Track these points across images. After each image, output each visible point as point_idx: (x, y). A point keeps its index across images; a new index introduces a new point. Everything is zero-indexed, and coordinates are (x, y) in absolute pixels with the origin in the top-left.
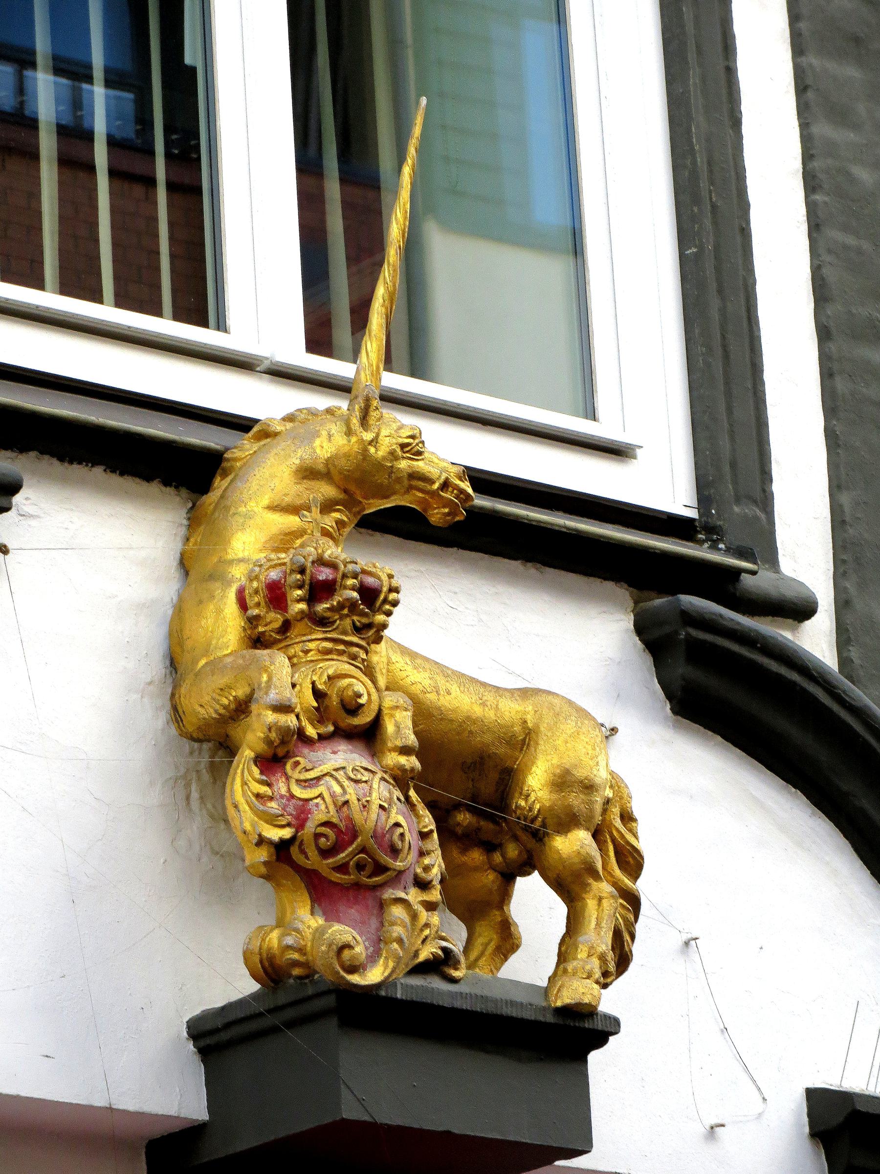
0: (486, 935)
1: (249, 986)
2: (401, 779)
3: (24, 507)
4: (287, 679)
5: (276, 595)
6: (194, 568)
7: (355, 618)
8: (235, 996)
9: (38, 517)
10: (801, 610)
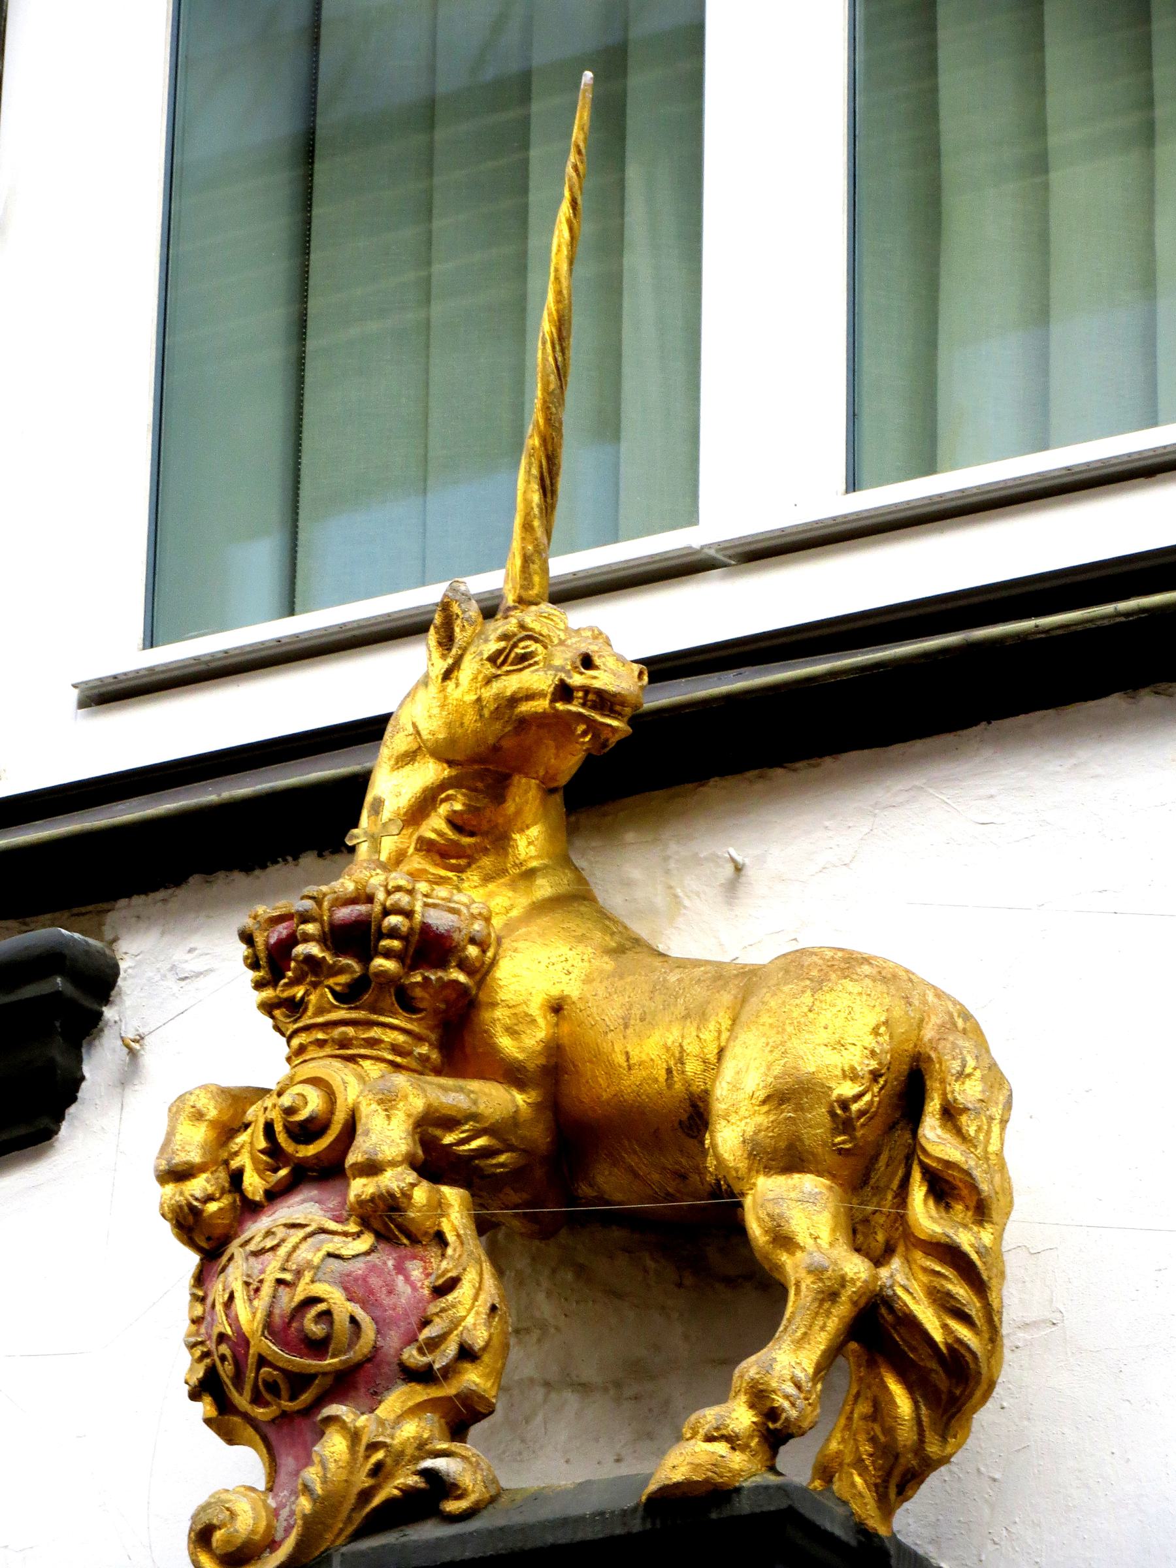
3: (184, 966)
7: (331, 982)
9: (211, 970)
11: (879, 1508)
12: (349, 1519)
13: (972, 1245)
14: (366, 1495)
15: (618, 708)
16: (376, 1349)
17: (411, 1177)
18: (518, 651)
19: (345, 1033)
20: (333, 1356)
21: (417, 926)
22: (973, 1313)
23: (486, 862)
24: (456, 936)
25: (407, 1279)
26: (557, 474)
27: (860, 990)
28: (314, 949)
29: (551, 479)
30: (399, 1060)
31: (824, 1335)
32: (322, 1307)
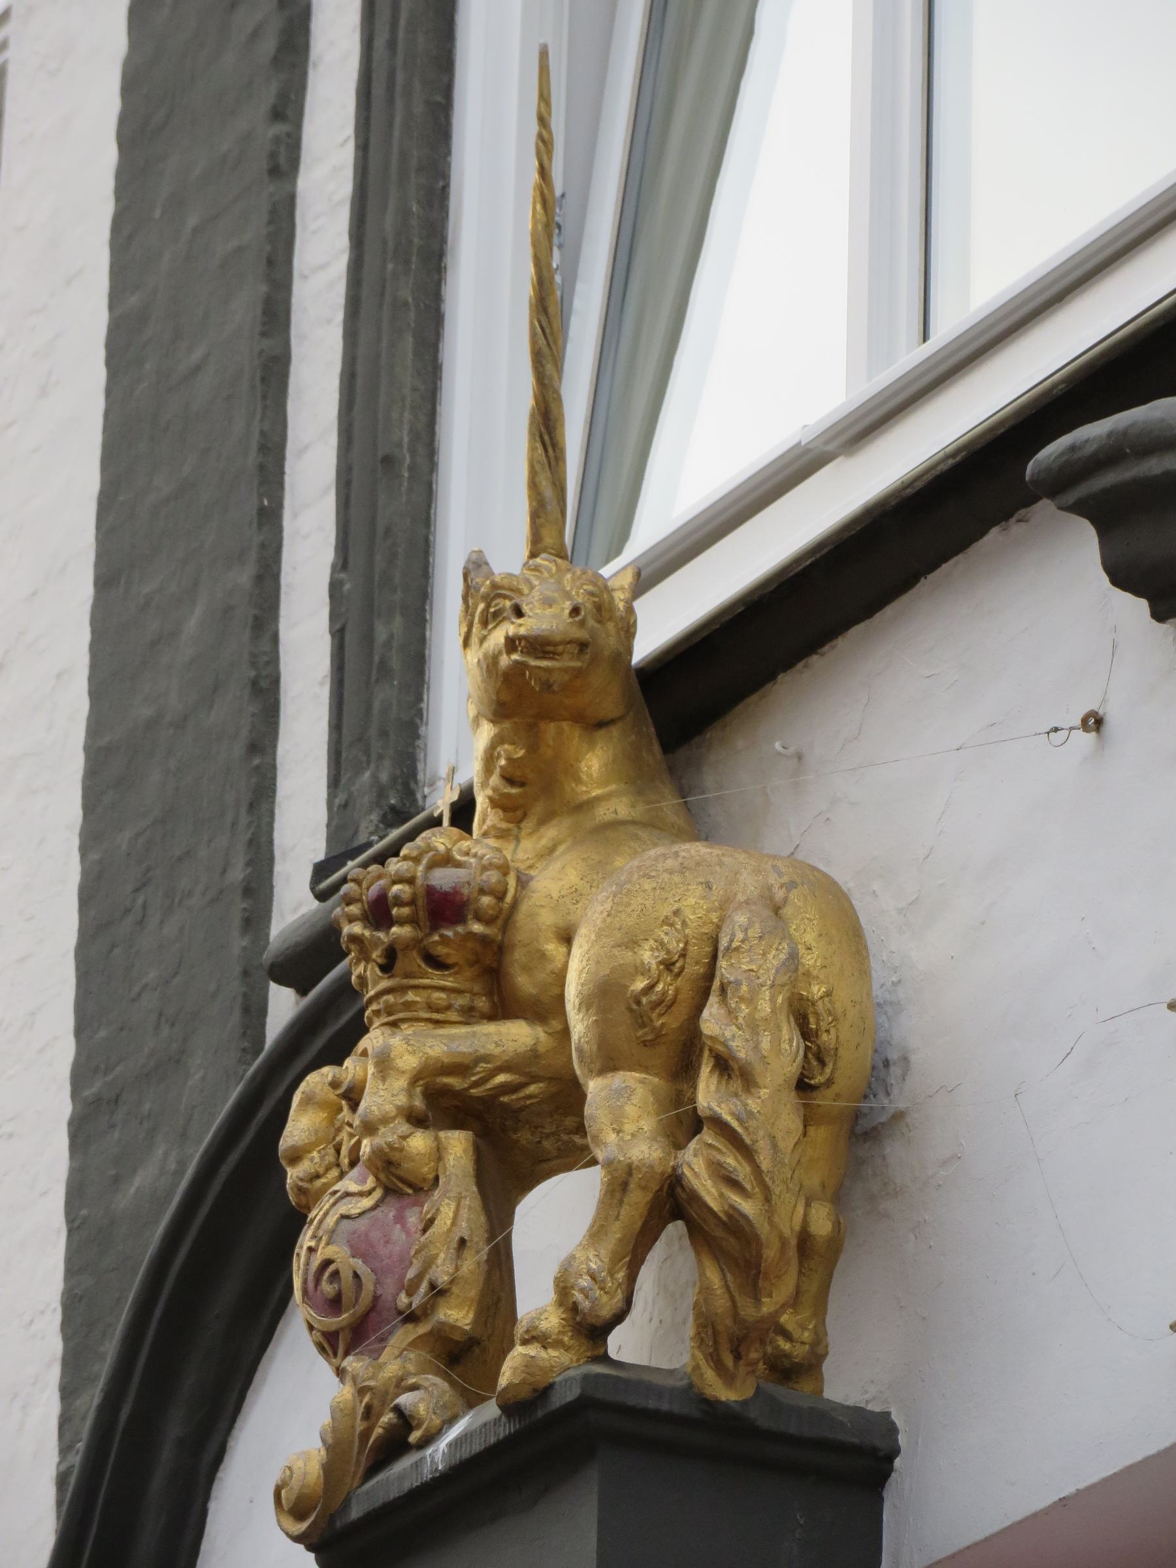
11: (719, 1375)
12: (358, 1461)
13: (732, 1114)
14: (365, 1435)
15: (550, 648)
16: (376, 1298)
17: (405, 1128)
18: (492, 610)
19: (386, 1002)
20: (346, 1311)
21: (421, 891)
22: (740, 1178)
23: (539, 809)
24: (465, 891)
25: (404, 1226)
26: (555, 429)
27: (654, 885)
28: (357, 928)
29: (550, 434)
30: (435, 1016)
31: (618, 1224)
32: (332, 1268)
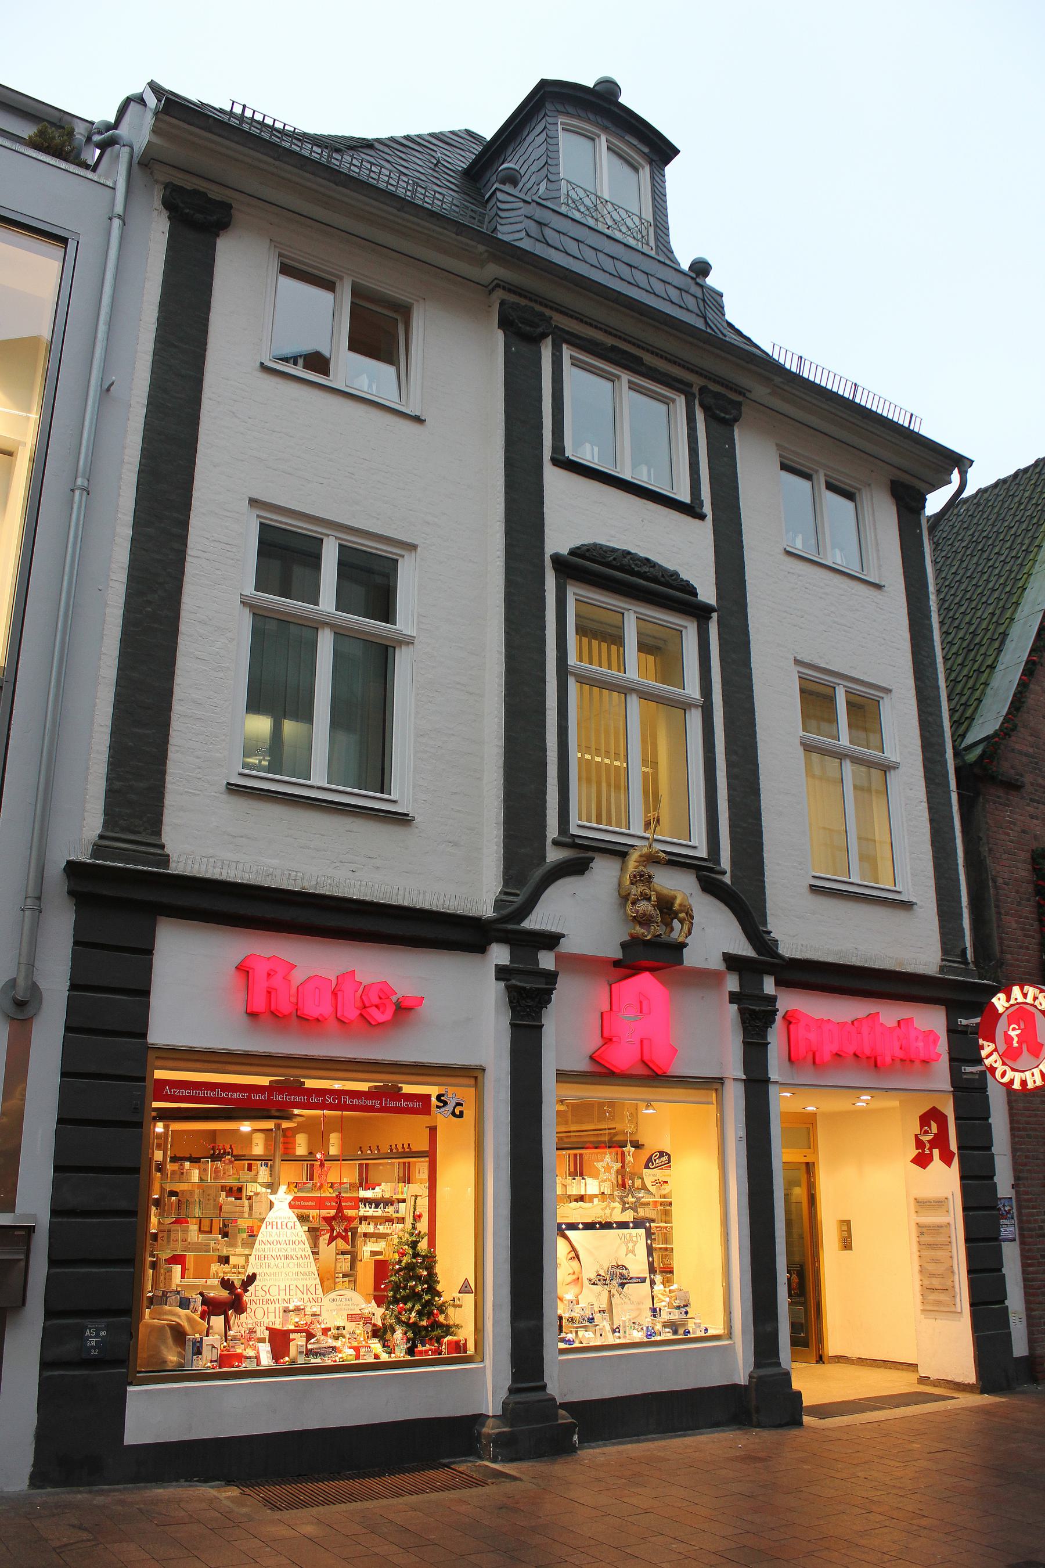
0: (668, 930)
1: (735, 1007)
2: (654, 906)
4: (636, 890)
5: (635, 876)
6: (623, 869)
8: (708, 601)
10: (724, 873)
